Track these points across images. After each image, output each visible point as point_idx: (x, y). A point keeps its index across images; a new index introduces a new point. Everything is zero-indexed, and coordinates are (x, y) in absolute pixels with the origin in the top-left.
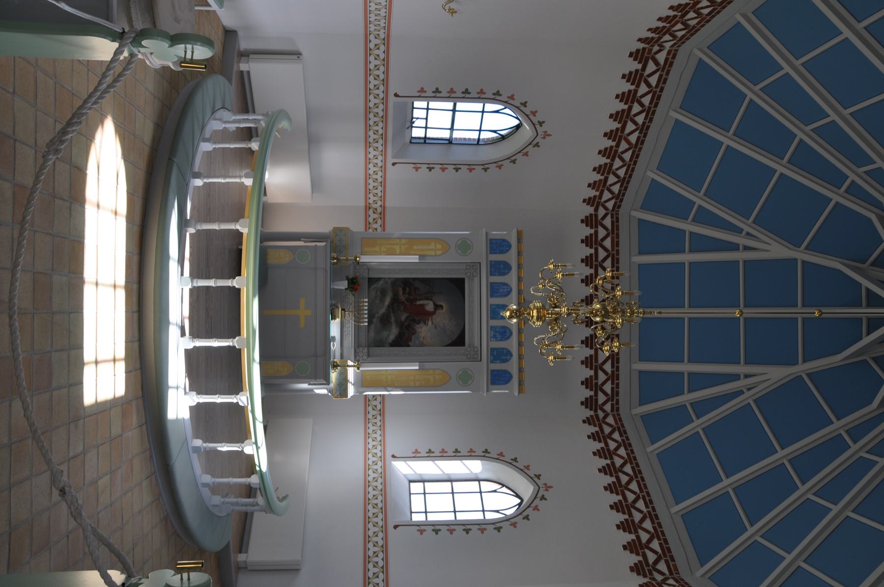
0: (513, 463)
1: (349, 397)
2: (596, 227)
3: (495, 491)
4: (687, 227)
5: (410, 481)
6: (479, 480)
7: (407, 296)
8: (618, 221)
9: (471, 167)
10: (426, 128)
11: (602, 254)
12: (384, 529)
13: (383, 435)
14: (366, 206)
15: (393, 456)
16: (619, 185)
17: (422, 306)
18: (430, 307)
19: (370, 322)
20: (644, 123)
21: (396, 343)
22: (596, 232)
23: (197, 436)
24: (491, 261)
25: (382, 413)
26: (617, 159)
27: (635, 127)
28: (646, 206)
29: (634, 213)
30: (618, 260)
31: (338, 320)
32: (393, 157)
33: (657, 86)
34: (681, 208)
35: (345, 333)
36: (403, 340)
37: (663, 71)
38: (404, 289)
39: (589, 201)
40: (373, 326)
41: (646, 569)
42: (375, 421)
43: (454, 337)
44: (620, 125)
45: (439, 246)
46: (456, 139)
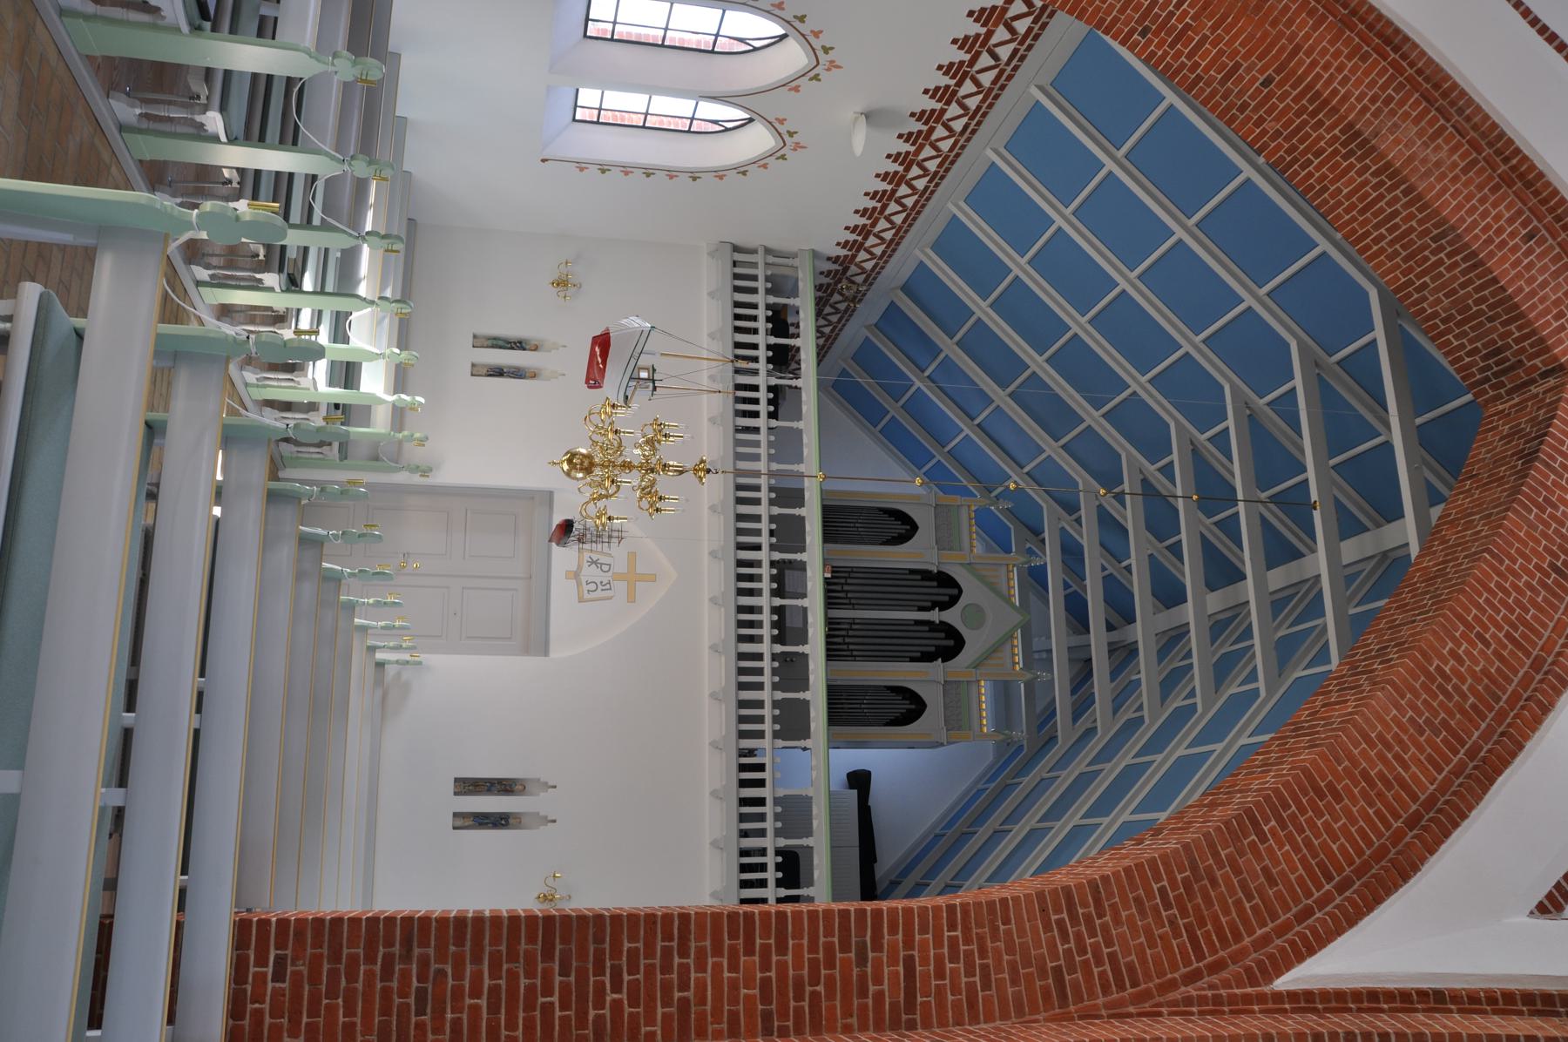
26: (954, 104)
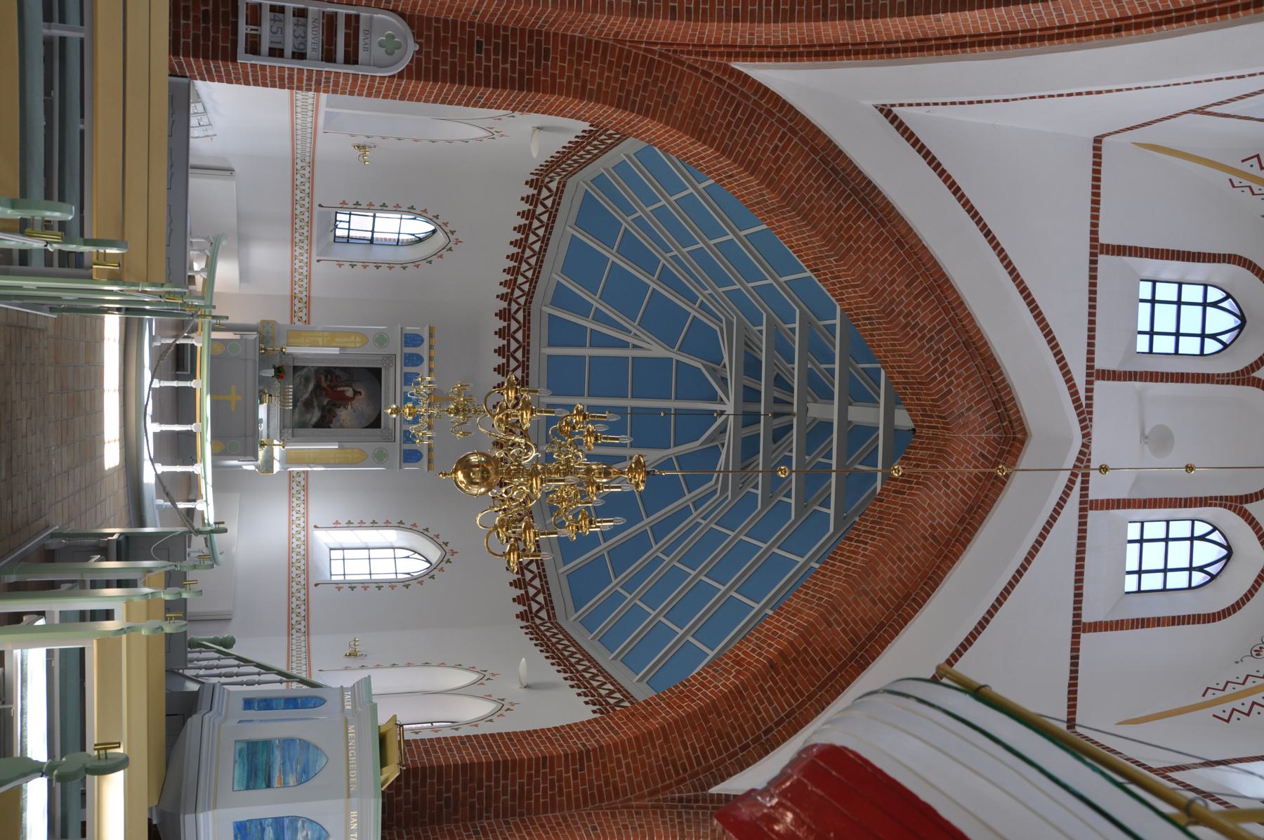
0: (424, 532)
1: (275, 472)
2: (509, 320)
3: (408, 557)
4: (590, 325)
5: (331, 549)
6: (394, 548)
7: (329, 383)
8: (529, 315)
9: (391, 266)
10: (349, 229)
11: (514, 345)
12: (306, 587)
13: (307, 508)
14: (292, 296)
15: (315, 527)
16: (528, 284)
17: (343, 392)
18: (350, 393)
19: (295, 406)
20: (544, 236)
21: (317, 426)
22: (509, 325)
23: (158, 497)
24: (405, 354)
25: (306, 488)
27: (536, 238)
28: (555, 303)
29: (544, 309)
30: (528, 350)
31: (265, 405)
32: (318, 255)
33: (552, 207)
34: (582, 308)
35: (271, 416)
36: (324, 422)
37: (556, 195)
38: (326, 377)
39: (502, 297)
40: (297, 409)
41: (529, 615)
42: (299, 496)
43: (371, 420)
44: (523, 236)
45: (358, 339)
46: (377, 239)
